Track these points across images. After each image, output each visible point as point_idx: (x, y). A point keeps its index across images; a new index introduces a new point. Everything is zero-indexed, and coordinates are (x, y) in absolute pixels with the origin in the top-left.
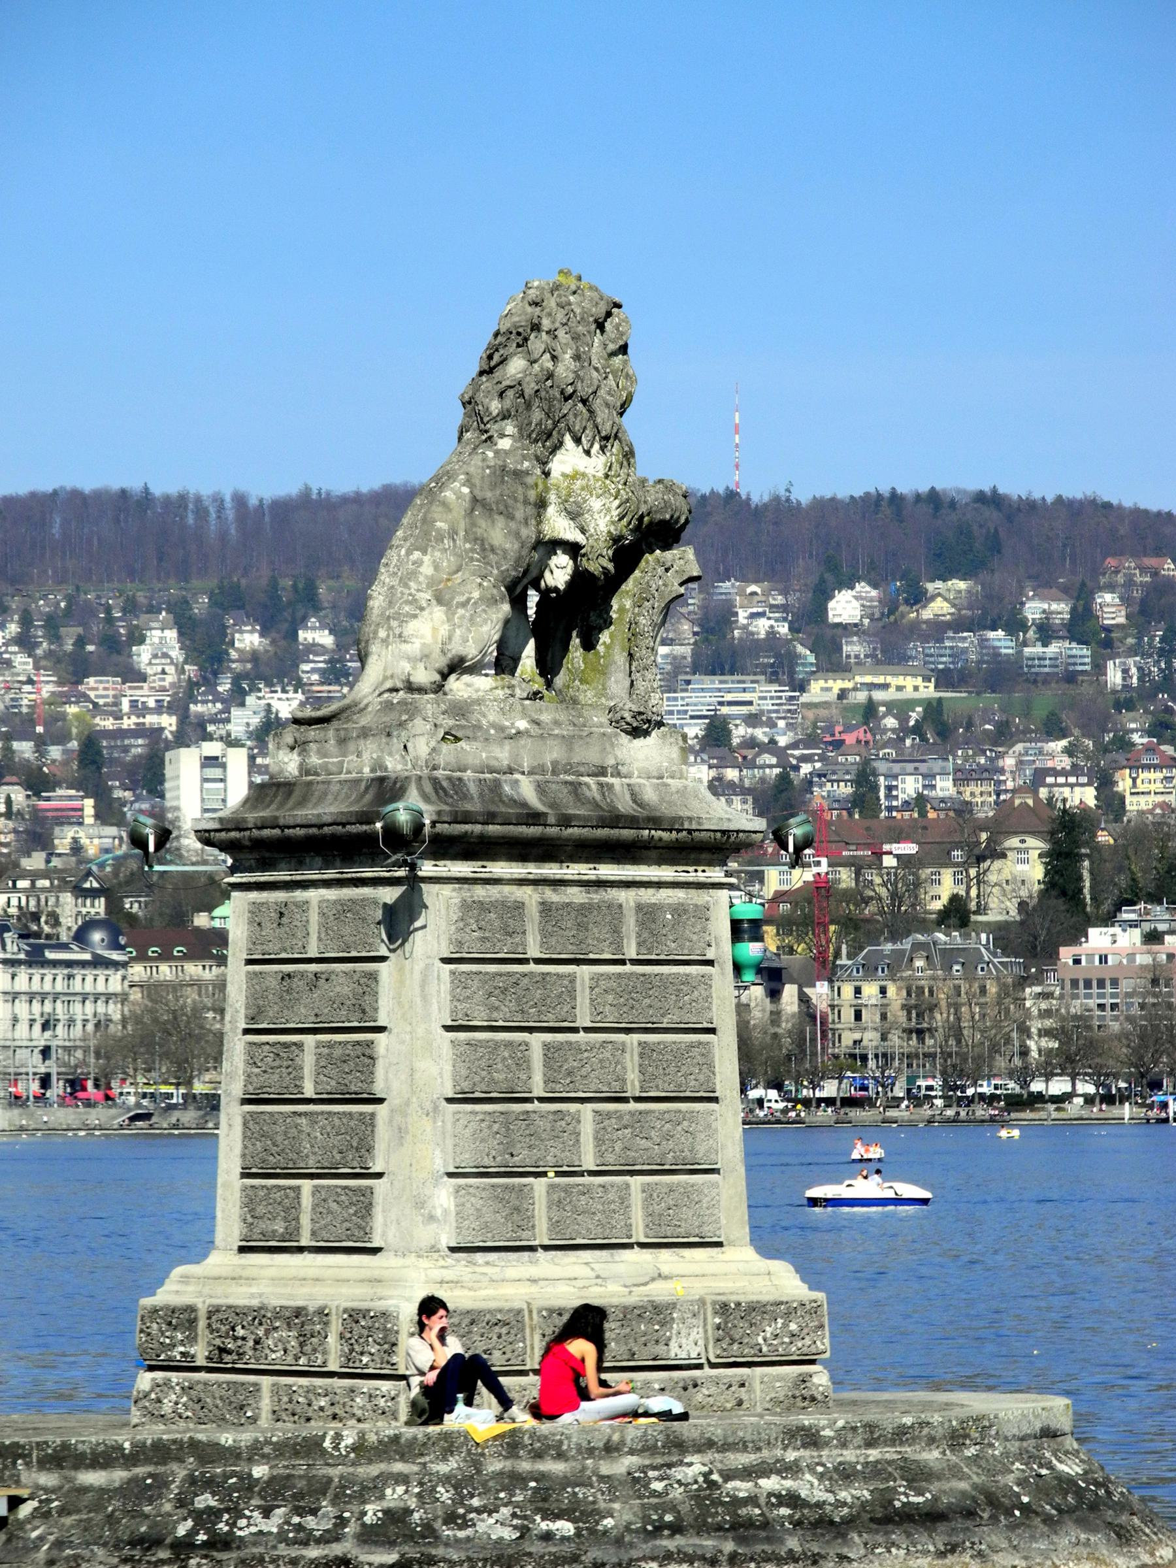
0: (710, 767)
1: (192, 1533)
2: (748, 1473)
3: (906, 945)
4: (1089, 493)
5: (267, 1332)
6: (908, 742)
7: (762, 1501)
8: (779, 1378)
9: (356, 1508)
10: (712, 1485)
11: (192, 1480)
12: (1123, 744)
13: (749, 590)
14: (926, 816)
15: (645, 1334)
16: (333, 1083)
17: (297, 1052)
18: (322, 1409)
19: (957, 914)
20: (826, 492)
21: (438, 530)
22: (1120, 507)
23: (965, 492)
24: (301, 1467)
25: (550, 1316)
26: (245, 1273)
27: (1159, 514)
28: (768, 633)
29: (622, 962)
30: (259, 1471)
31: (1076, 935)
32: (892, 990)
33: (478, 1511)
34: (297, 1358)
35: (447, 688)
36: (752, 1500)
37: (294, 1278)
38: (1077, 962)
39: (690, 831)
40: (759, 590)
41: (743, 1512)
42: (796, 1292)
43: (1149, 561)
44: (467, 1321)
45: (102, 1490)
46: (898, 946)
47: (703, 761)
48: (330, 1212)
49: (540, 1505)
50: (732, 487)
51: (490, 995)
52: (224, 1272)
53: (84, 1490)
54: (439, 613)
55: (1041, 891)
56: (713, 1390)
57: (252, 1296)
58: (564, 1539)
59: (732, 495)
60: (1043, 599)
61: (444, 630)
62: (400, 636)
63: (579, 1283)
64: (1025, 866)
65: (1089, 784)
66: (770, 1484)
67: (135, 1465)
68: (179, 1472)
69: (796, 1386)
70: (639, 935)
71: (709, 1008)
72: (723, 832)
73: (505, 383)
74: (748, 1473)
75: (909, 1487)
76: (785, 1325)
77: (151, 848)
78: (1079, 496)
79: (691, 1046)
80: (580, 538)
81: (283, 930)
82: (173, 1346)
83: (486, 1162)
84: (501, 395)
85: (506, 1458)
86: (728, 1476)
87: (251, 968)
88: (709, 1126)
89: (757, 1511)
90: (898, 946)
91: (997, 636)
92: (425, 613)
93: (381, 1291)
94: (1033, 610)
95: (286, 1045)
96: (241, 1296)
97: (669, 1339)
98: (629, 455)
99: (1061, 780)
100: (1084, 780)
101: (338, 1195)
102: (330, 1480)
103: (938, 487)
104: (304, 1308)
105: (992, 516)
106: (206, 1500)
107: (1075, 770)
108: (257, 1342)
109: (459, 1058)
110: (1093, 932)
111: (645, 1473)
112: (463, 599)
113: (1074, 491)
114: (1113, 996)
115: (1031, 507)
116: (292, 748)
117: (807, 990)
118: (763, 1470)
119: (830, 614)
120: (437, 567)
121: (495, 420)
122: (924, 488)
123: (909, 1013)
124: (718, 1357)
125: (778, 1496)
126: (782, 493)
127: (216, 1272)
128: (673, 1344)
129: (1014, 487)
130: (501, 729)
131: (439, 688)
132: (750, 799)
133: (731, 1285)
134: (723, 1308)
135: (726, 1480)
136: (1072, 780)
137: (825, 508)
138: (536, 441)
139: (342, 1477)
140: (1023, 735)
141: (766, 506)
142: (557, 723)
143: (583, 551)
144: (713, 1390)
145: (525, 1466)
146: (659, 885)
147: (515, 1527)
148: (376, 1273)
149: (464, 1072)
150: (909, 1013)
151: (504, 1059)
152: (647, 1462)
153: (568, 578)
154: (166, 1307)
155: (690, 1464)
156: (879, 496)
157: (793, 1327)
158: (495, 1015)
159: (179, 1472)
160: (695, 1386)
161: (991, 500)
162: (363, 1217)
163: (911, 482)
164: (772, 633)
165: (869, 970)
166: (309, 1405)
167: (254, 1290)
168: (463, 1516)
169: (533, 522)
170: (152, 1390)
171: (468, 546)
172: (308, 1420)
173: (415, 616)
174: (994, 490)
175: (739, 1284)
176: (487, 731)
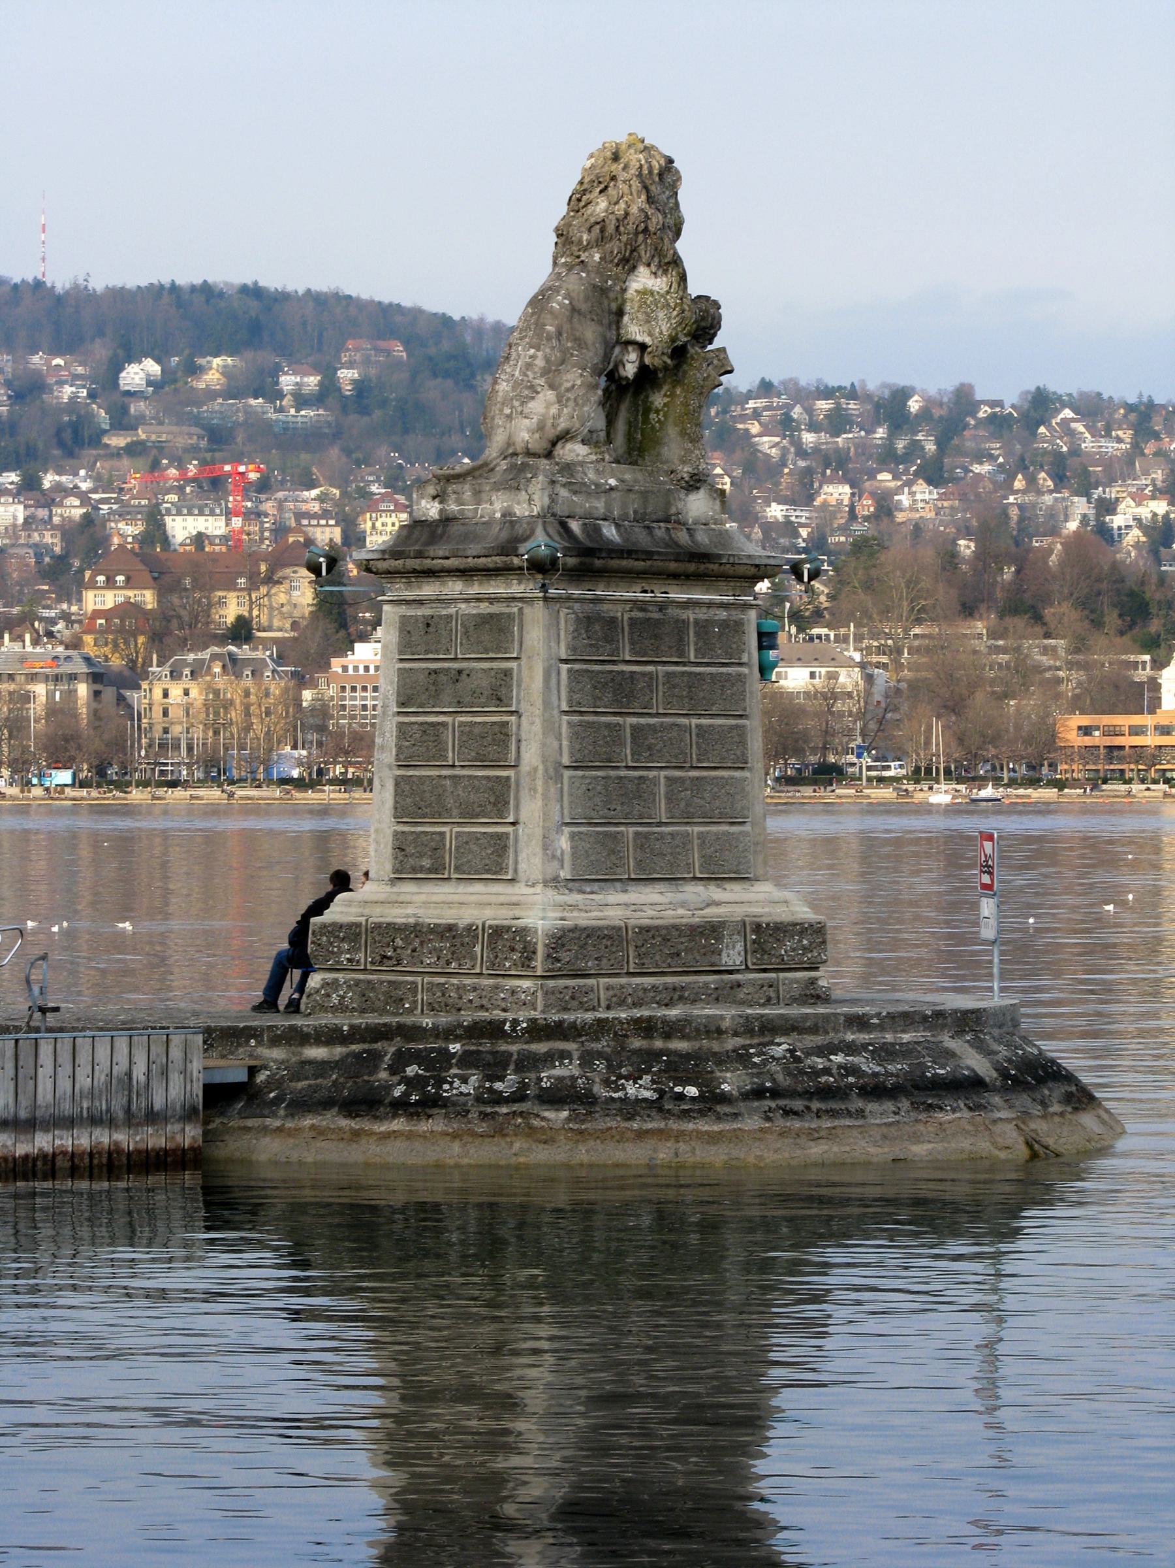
0: (25, 507)
1: (406, 1094)
2: (821, 1051)
3: (206, 655)
4: (332, 287)
5: (422, 943)
6: (188, 490)
7: (834, 1071)
8: (796, 981)
9: (533, 1076)
10: (798, 1060)
11: (399, 1054)
12: (365, 494)
13: (54, 362)
14: (203, 549)
15: (705, 947)
16: (473, 754)
17: (442, 729)
18: (471, 1001)
19: (242, 631)
20: (117, 281)
21: (548, 333)
22: (358, 299)
23: (232, 285)
24: (486, 1046)
25: (640, 932)
26: (401, 898)
27: (391, 305)
28: (70, 398)
29: (684, 664)
30: (455, 1047)
31: (347, 646)
32: (194, 693)
33: (627, 1078)
34: (448, 963)
35: (555, 453)
36: (827, 1071)
37: (444, 903)
38: (345, 669)
39: (733, 564)
40: (62, 363)
41: (823, 1079)
42: (806, 916)
43: (382, 344)
44: (584, 935)
45: (323, 1062)
46: (200, 656)
47: (20, 502)
48: (470, 851)
49: (672, 1074)
50: (40, 277)
51: (595, 688)
52: (381, 897)
53: (310, 1062)
54: (550, 395)
55: (311, 612)
56: (751, 990)
57: (407, 916)
58: (693, 1099)
59: (38, 285)
60: (295, 373)
61: (554, 410)
62: (521, 413)
63: (659, 908)
64: (300, 593)
65: (336, 525)
66: (838, 1059)
67: (352, 1043)
68: (390, 1049)
69: (807, 987)
70: (696, 644)
71: (744, 700)
72: (757, 566)
73: (592, 220)
74: (821, 1051)
75: (934, 1062)
76: (800, 941)
77: (324, 573)
78: (325, 289)
79: (732, 728)
80: (647, 340)
81: (430, 637)
82: (340, 952)
83: (593, 814)
84: (589, 230)
85: (643, 1038)
86: (808, 1053)
87: (401, 665)
88: (743, 789)
89: (832, 1079)
90: (200, 656)
91: (256, 402)
92: (541, 395)
93: (517, 912)
94: (287, 381)
95: (432, 724)
96: (397, 915)
97: (721, 950)
98: (683, 278)
99: (314, 522)
100: (332, 522)
101: (478, 839)
102: (511, 1055)
103: (210, 281)
104: (455, 925)
105: (254, 305)
106: (411, 1070)
107: (325, 514)
108: (414, 951)
109: (575, 736)
110: (357, 646)
111: (747, 1051)
112: (569, 385)
113: (321, 285)
114: (374, 698)
115: (283, 297)
116: (434, 498)
117: (127, 693)
118: (833, 1049)
119: (121, 382)
120: (547, 360)
121: (585, 249)
122: (198, 281)
123: (208, 709)
124: (754, 964)
125: (845, 1068)
126: (81, 281)
127: (366, 898)
128: (724, 954)
129: (272, 281)
130: (597, 485)
131: (549, 455)
132: (59, 534)
133: (760, 910)
134: (758, 928)
135: (806, 1057)
136: (323, 522)
137: (118, 295)
138: (617, 265)
139: (519, 1053)
140: (282, 485)
141: (67, 293)
142: (636, 481)
143: (649, 350)
144: (751, 990)
145: (659, 1044)
146: (710, 605)
147: (655, 1090)
148: (514, 899)
149: (578, 747)
150: (208, 709)
151: (605, 737)
152: (748, 1042)
153: (635, 370)
154: (334, 924)
155: (779, 1044)
156: (162, 287)
157: (805, 942)
158: (598, 703)
159: (390, 1049)
160: (739, 986)
161: (254, 292)
162: (500, 856)
163: (187, 275)
164: (74, 398)
165: (175, 675)
166: (460, 998)
167: (410, 911)
168: (615, 1082)
169: (614, 327)
170: (322, 987)
171: (569, 344)
172: (459, 1010)
173: (533, 398)
174: (256, 283)
175: (767, 910)
176: (589, 486)
